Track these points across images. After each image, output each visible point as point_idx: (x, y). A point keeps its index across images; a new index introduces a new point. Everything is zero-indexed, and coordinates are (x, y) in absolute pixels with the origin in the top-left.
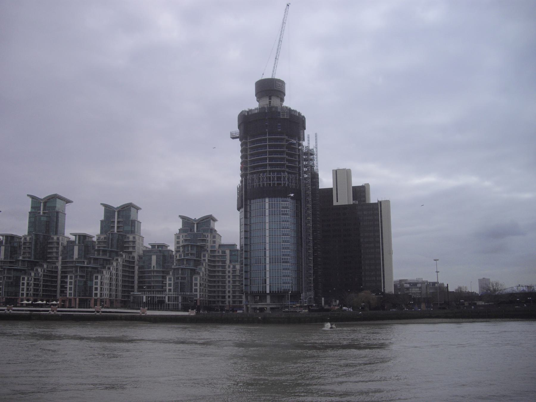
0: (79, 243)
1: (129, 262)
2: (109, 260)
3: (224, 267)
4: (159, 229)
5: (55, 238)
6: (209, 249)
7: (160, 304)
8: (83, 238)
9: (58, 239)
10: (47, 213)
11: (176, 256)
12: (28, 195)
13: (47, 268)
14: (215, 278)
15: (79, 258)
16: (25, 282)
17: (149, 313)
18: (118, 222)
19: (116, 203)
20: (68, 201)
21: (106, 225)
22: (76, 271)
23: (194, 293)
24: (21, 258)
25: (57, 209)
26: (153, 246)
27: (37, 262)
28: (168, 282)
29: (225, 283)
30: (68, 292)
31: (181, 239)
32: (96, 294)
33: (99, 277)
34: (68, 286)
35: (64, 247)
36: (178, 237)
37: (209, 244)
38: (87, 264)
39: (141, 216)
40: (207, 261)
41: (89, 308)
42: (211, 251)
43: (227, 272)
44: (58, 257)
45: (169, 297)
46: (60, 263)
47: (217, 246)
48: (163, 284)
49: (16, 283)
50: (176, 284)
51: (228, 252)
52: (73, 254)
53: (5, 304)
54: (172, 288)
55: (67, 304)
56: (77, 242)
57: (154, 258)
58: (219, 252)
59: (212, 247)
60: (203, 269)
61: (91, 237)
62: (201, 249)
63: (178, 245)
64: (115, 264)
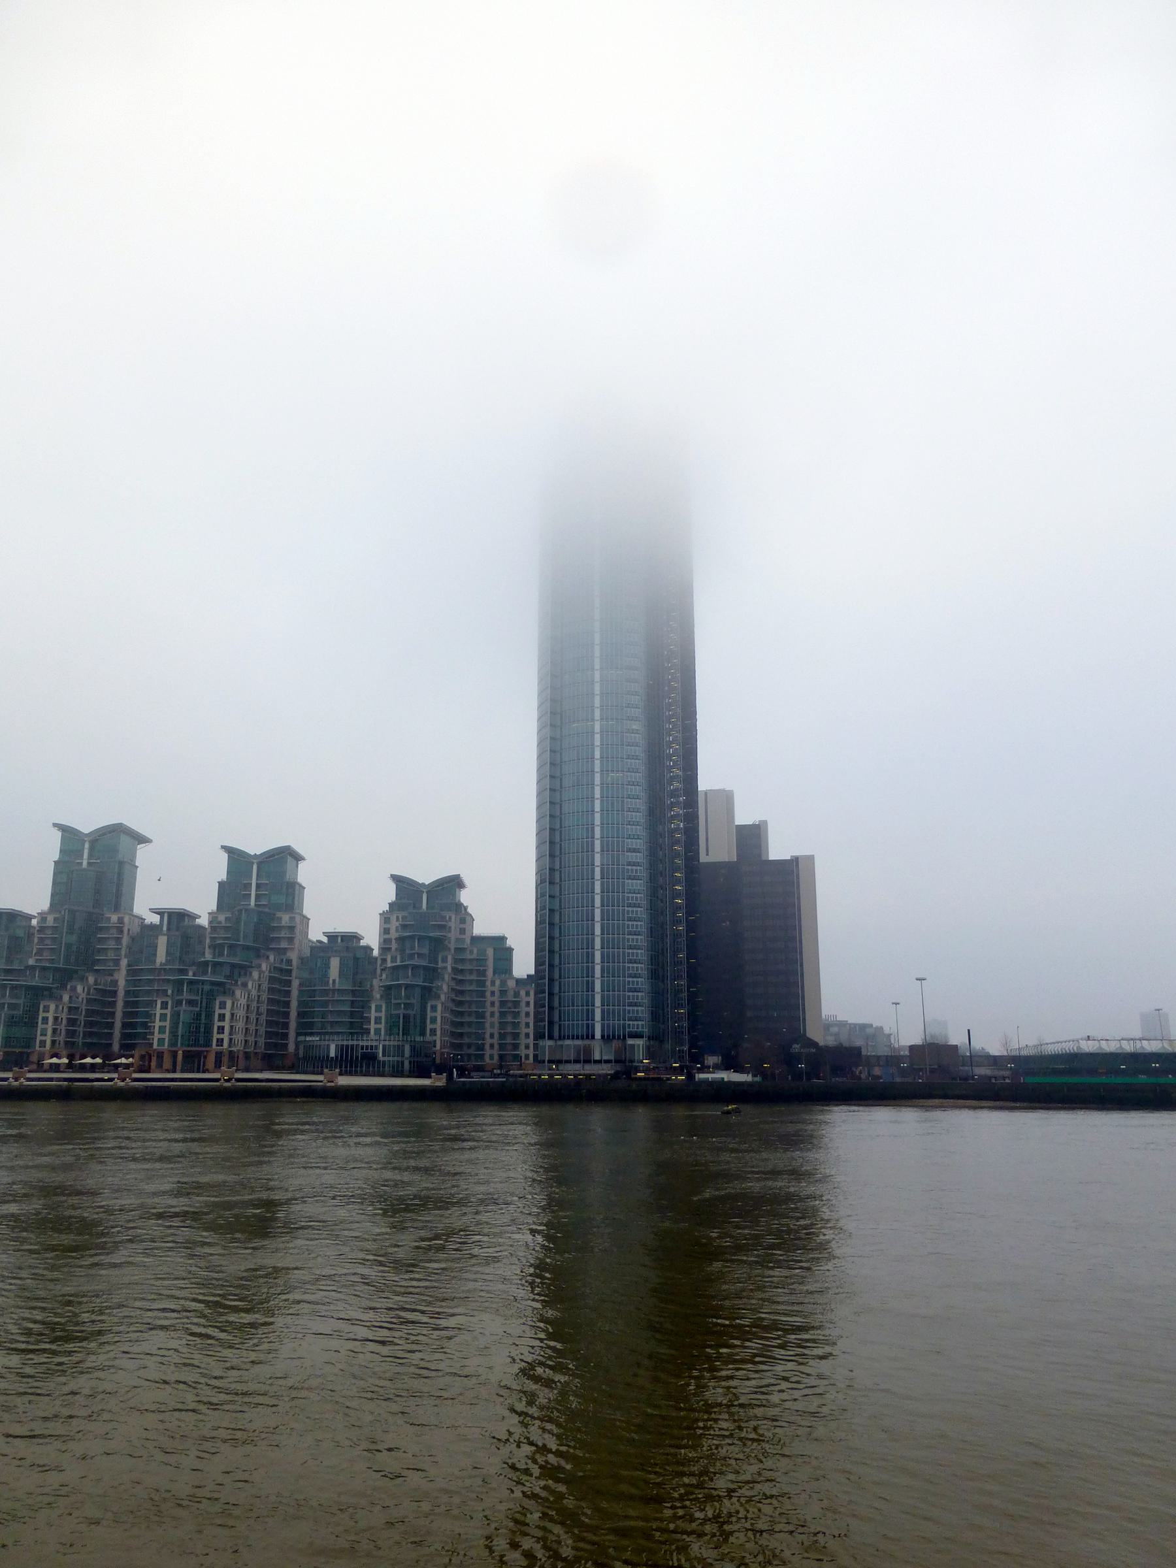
0: (169, 929)
1: (281, 970)
2: (242, 967)
3: (482, 983)
4: (343, 904)
5: (114, 918)
6: (452, 946)
7: (366, 1061)
8: (178, 919)
9: (121, 921)
10: (96, 865)
11: (384, 960)
12: (55, 825)
13: (96, 983)
14: (466, 1006)
15: (168, 962)
16: (51, 1016)
17: (344, 1081)
18: (258, 886)
19: (255, 846)
20: (143, 840)
21: (229, 892)
22: (180, 991)
23: (428, 1038)
24: (31, 962)
25: (120, 856)
26: (332, 937)
27: (76, 972)
28: (373, 1014)
29: (484, 1017)
30: (156, 1036)
31: (394, 924)
32: (220, 1042)
33: (229, 1004)
34: (158, 1024)
35: (133, 939)
36: (385, 918)
37: (453, 935)
38: (194, 975)
39: (304, 874)
40: (449, 969)
41: (204, 1072)
42: (456, 949)
43: (488, 994)
44: (119, 960)
45: (384, 1046)
46: (124, 972)
47: (468, 941)
48: (362, 1018)
49: (29, 1019)
50: (389, 1017)
51: (490, 952)
52: (155, 955)
53: (4, 1066)
54: (382, 1026)
55: (153, 1064)
56: (165, 928)
57: (335, 963)
58: (471, 952)
59: (457, 940)
60: (445, 988)
61: (193, 917)
62: (438, 944)
63: (387, 936)
64: (255, 975)
